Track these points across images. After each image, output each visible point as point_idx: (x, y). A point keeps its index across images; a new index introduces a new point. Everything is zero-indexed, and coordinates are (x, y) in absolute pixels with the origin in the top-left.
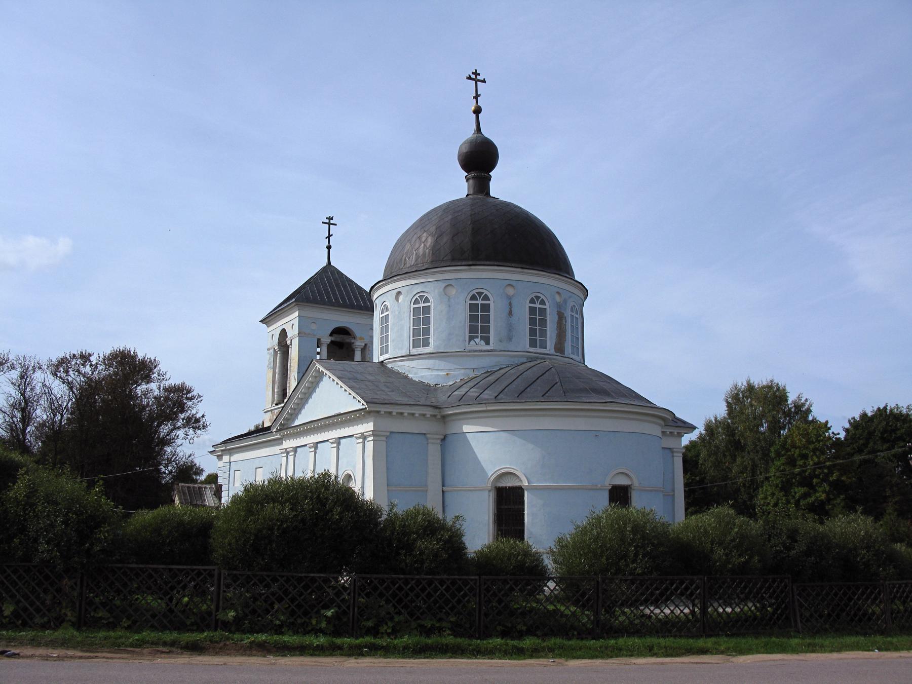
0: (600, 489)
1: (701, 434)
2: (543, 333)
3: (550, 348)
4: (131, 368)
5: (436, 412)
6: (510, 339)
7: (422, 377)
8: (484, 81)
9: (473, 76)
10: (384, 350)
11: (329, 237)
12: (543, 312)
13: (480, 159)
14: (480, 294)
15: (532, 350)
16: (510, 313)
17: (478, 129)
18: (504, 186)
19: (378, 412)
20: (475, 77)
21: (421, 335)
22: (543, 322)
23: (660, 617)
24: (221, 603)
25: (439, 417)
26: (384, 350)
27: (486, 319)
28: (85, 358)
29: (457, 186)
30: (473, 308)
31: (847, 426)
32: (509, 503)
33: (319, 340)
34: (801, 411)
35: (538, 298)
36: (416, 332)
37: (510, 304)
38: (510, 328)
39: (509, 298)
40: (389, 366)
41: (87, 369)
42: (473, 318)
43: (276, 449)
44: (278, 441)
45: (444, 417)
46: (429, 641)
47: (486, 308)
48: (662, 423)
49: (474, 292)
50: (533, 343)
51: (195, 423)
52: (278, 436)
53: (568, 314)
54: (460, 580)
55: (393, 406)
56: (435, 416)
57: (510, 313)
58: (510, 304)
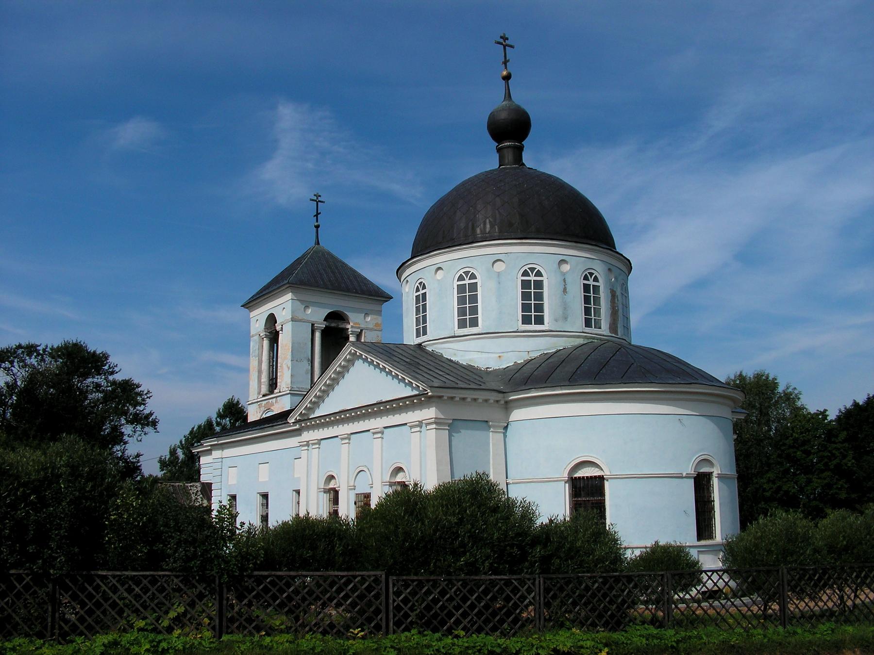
0: (686, 477)
1: (824, 414)
2: (597, 312)
3: (605, 329)
4: (80, 360)
5: (499, 396)
6: (565, 318)
7: (470, 360)
8: (512, 47)
9: (502, 41)
10: (422, 331)
11: (316, 216)
12: (596, 289)
13: (511, 130)
14: (532, 269)
15: (588, 330)
16: (565, 290)
17: (508, 96)
18: (533, 158)
19: (440, 397)
20: (504, 42)
21: (468, 314)
22: (597, 301)
23: (698, 612)
24: (391, 615)
25: (502, 402)
26: (422, 331)
27: (539, 297)
28: (31, 349)
29: (486, 159)
30: (525, 284)
31: (843, 409)
32: (587, 492)
33: (313, 325)
34: (789, 398)
35: (591, 274)
36: (462, 312)
37: (564, 280)
38: (565, 307)
39: (564, 274)
40: (429, 349)
41: (33, 361)
42: (525, 296)
43: (293, 441)
44: (297, 432)
45: (506, 402)
46: (234, 638)
47: (539, 285)
48: (731, 403)
49: (526, 268)
50: (588, 323)
51: (147, 421)
52: (297, 427)
53: (618, 293)
54: (114, 577)
55: (468, 392)
56: (497, 401)
57: (565, 290)
58: (564, 280)
